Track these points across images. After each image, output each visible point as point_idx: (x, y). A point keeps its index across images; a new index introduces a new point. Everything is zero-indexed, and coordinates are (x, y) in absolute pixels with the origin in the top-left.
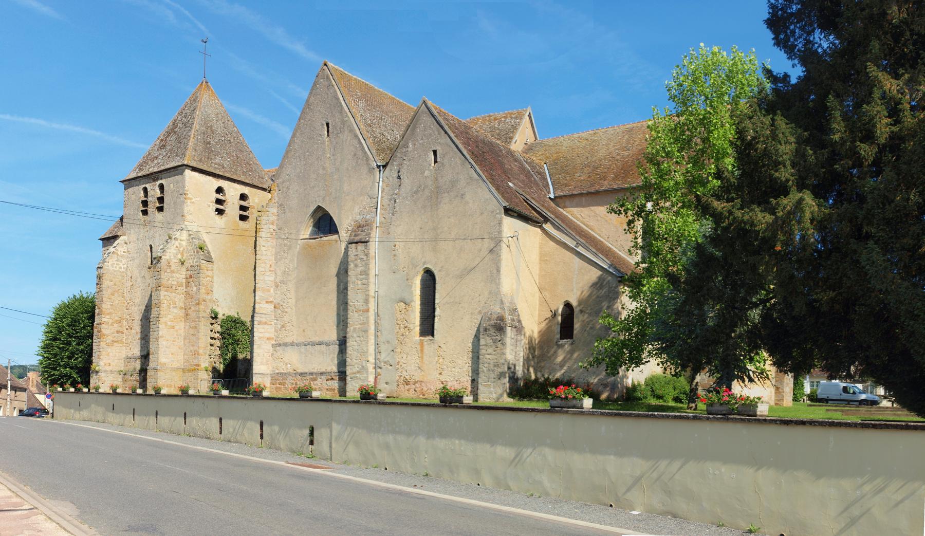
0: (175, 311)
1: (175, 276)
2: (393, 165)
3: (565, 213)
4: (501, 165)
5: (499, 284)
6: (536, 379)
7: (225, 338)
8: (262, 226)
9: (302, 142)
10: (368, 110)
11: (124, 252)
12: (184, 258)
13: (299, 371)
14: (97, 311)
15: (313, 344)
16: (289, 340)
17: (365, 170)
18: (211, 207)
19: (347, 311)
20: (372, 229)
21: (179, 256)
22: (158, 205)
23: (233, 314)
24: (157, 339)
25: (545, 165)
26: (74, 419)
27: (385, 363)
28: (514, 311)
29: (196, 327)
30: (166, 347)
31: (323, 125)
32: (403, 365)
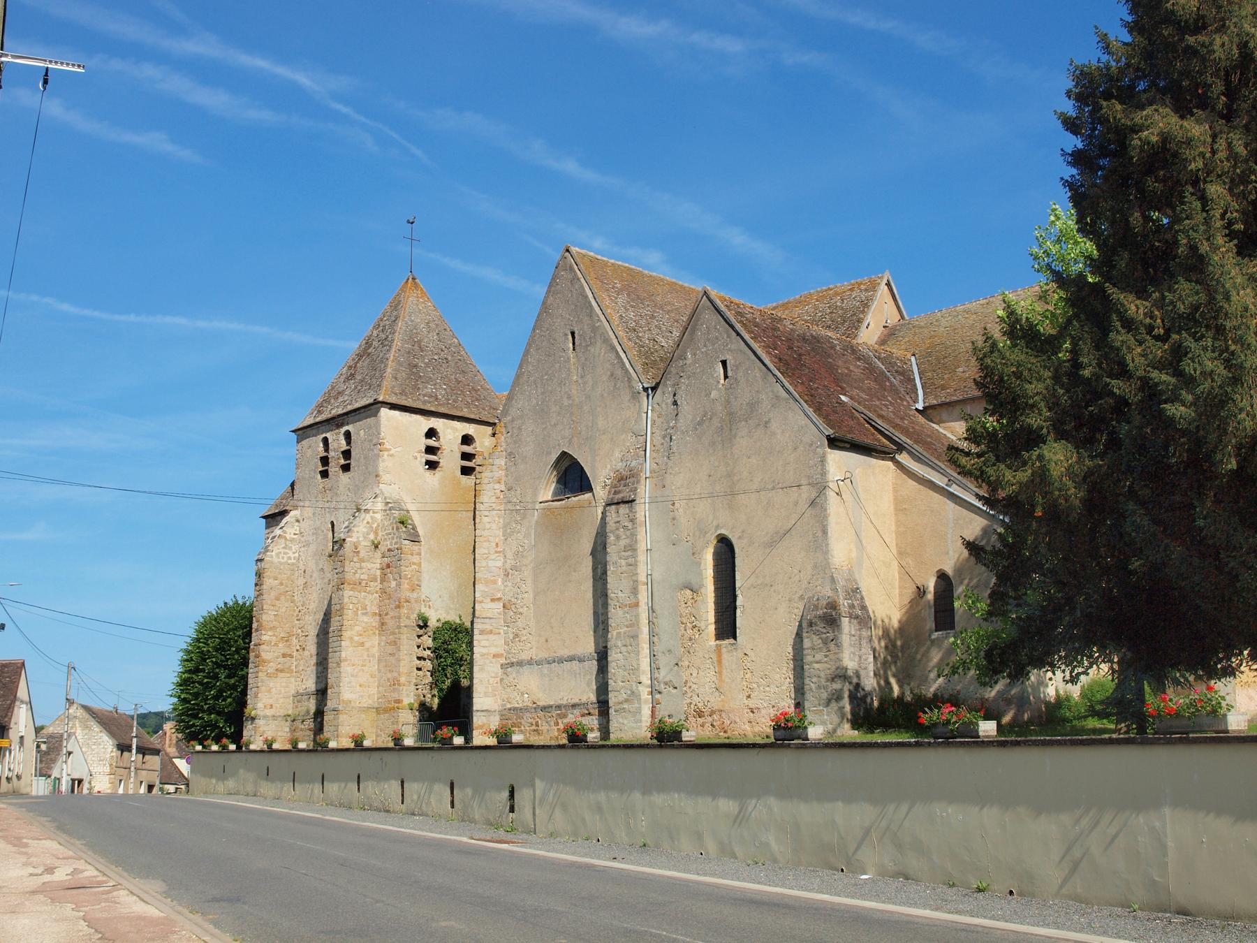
0: (366, 619)
1: (367, 567)
2: (665, 385)
3: (941, 430)
4: (831, 369)
5: (827, 552)
6: (901, 697)
7: (441, 657)
8: (484, 487)
9: (539, 361)
10: (632, 306)
11: (295, 534)
12: (379, 538)
13: (541, 703)
14: (255, 626)
15: (561, 661)
16: (525, 656)
17: (626, 396)
18: (419, 459)
19: (607, 608)
20: (638, 482)
21: (372, 537)
22: (342, 462)
23: (453, 618)
24: (338, 664)
25: (913, 359)
26: (215, 793)
27: (666, 684)
28: (854, 592)
29: (395, 643)
30: (352, 676)
31: (566, 335)
32: (694, 686)
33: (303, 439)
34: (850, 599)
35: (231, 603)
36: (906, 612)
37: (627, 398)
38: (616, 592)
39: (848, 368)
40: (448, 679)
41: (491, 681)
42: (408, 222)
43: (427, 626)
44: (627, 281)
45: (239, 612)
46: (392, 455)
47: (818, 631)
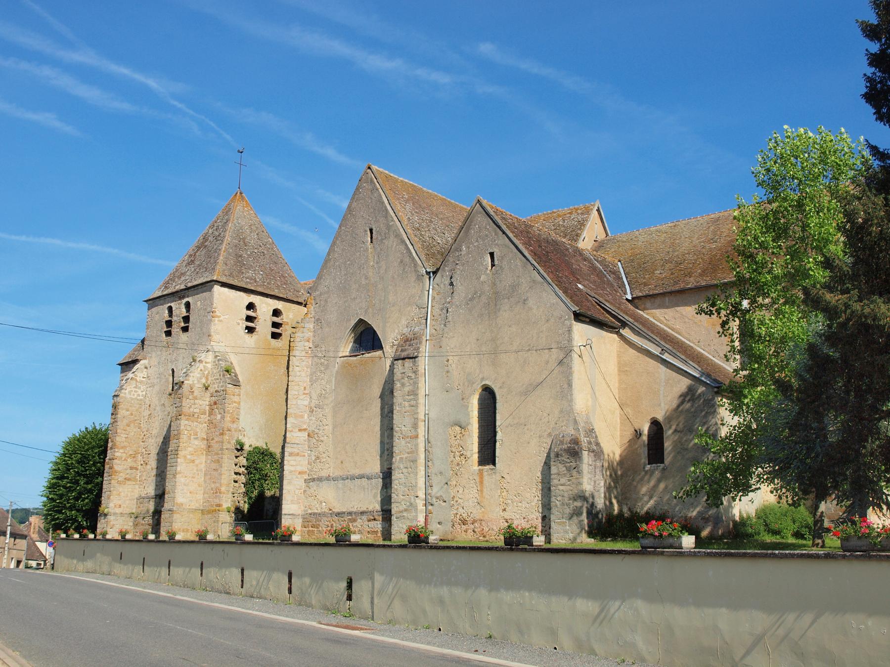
0: (196, 442)
3: (645, 315)
4: (569, 265)
5: (571, 400)
7: (251, 473)
10: (416, 212)
11: (143, 378)
12: (209, 382)
13: (336, 510)
14: (110, 445)
15: (353, 478)
16: (324, 474)
17: (413, 277)
18: (241, 325)
20: (421, 343)
21: (204, 381)
22: (183, 325)
23: (261, 444)
24: (174, 476)
25: (619, 263)
26: (75, 571)
28: (591, 431)
29: (218, 461)
30: (185, 485)
31: (366, 231)
33: (152, 307)
34: (588, 437)
35: (91, 429)
36: (625, 450)
37: (413, 279)
38: (400, 426)
39: (579, 265)
40: (256, 490)
41: (297, 492)
42: (239, 151)
43: (243, 450)
44: (412, 194)
45: (97, 435)
46: (221, 321)
47: (563, 461)
